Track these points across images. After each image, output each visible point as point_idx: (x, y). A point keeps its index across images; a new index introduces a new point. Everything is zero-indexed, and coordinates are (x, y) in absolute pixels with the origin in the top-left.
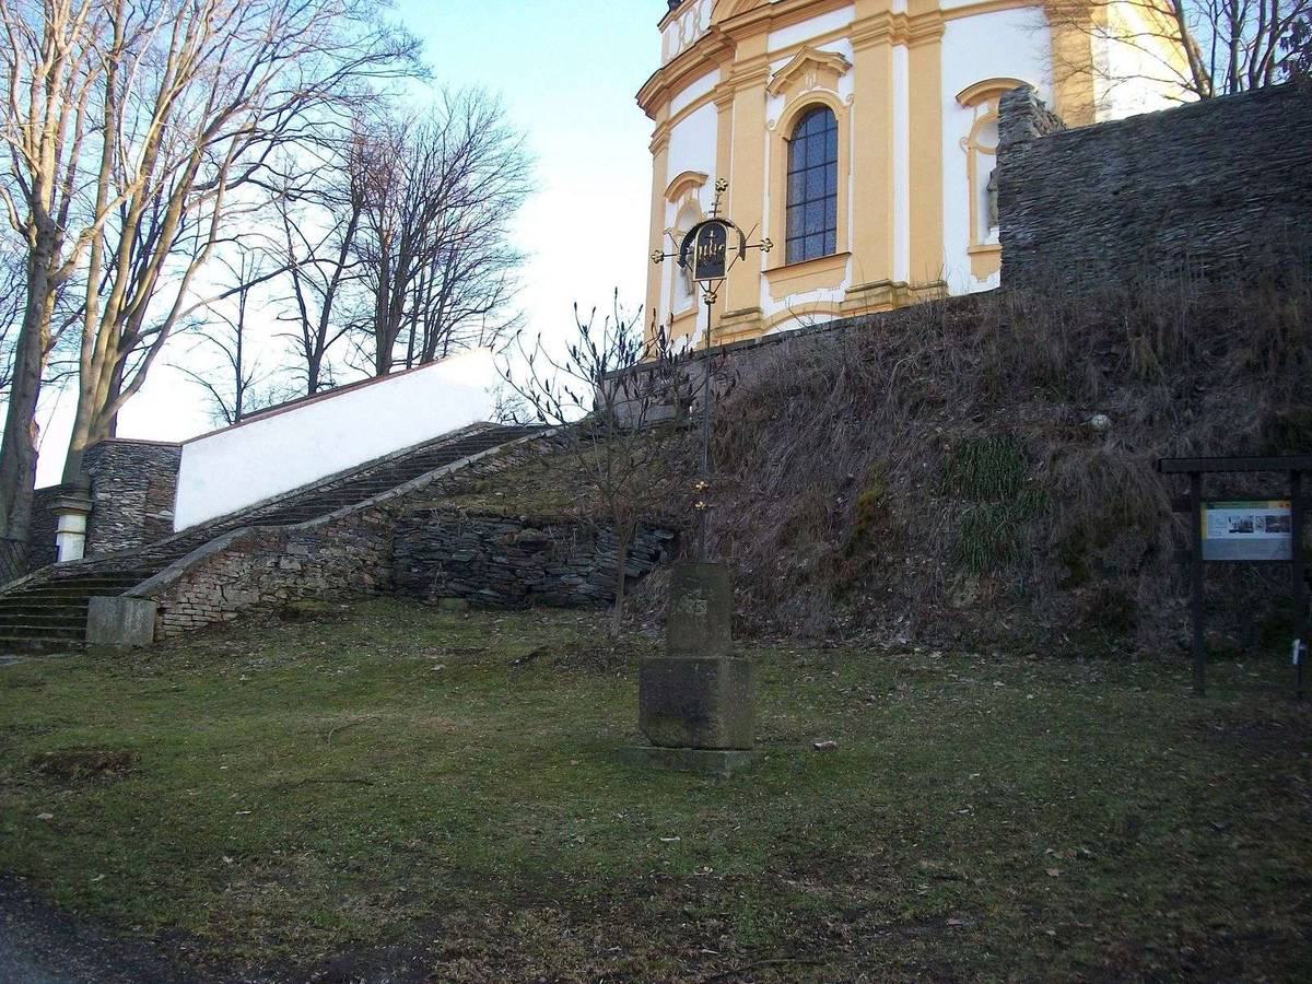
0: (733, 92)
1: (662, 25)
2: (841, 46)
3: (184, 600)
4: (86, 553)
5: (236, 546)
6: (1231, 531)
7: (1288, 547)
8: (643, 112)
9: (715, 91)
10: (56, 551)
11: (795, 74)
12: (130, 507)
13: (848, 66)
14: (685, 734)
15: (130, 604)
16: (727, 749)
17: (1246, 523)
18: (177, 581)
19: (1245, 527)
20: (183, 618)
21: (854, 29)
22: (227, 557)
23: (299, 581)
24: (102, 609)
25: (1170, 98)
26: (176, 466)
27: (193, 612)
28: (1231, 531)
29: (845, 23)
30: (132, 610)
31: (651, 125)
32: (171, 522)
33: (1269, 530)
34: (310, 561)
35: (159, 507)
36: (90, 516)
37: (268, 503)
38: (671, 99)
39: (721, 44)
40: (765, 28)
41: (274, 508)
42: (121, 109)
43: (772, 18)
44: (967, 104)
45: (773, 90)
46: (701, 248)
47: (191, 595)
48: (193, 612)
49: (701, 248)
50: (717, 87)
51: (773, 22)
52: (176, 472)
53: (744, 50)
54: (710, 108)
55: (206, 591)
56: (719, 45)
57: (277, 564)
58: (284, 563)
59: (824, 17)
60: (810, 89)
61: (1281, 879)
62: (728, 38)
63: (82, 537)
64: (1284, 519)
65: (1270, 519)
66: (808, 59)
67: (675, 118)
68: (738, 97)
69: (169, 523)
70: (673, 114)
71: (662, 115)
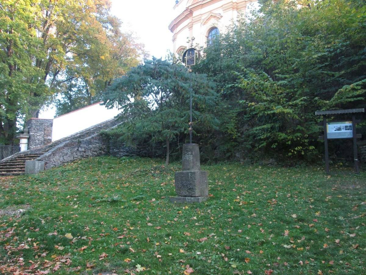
0: (192, 25)
1: (174, 8)
2: (220, 11)
3: (52, 160)
4: (28, 149)
5: (66, 146)
6: (335, 130)
7: (352, 134)
8: (170, 31)
9: (188, 25)
10: (20, 149)
11: (208, 19)
12: (39, 136)
13: (222, 17)
14: (187, 193)
15: (37, 162)
16: (200, 196)
17: (339, 128)
18: (50, 155)
20: (52, 165)
21: (223, 7)
22: (64, 148)
23: (84, 154)
24: (29, 163)
26: (51, 125)
27: (55, 163)
28: (335, 130)
29: (187, 24)
30: (37, 164)
31: (172, 34)
32: (51, 140)
33: (346, 129)
34: (87, 148)
35: (47, 136)
36: (29, 139)
37: (77, 134)
39: (189, 12)
40: (200, 7)
41: (79, 135)
43: (202, 5)
45: (203, 24)
47: (54, 159)
48: (55, 163)
50: (188, 24)
51: (202, 6)
52: (52, 127)
53: (195, 13)
54: (187, 29)
55: (59, 158)
56: (189, 12)
57: (78, 150)
58: (80, 149)
59: (184, 22)
60: (212, 22)
62: (191, 11)
63: (27, 145)
64: (350, 126)
65: (346, 127)
66: (211, 15)
67: (178, 32)
68: (194, 26)
69: (50, 140)
70: (177, 32)
71: (175, 31)
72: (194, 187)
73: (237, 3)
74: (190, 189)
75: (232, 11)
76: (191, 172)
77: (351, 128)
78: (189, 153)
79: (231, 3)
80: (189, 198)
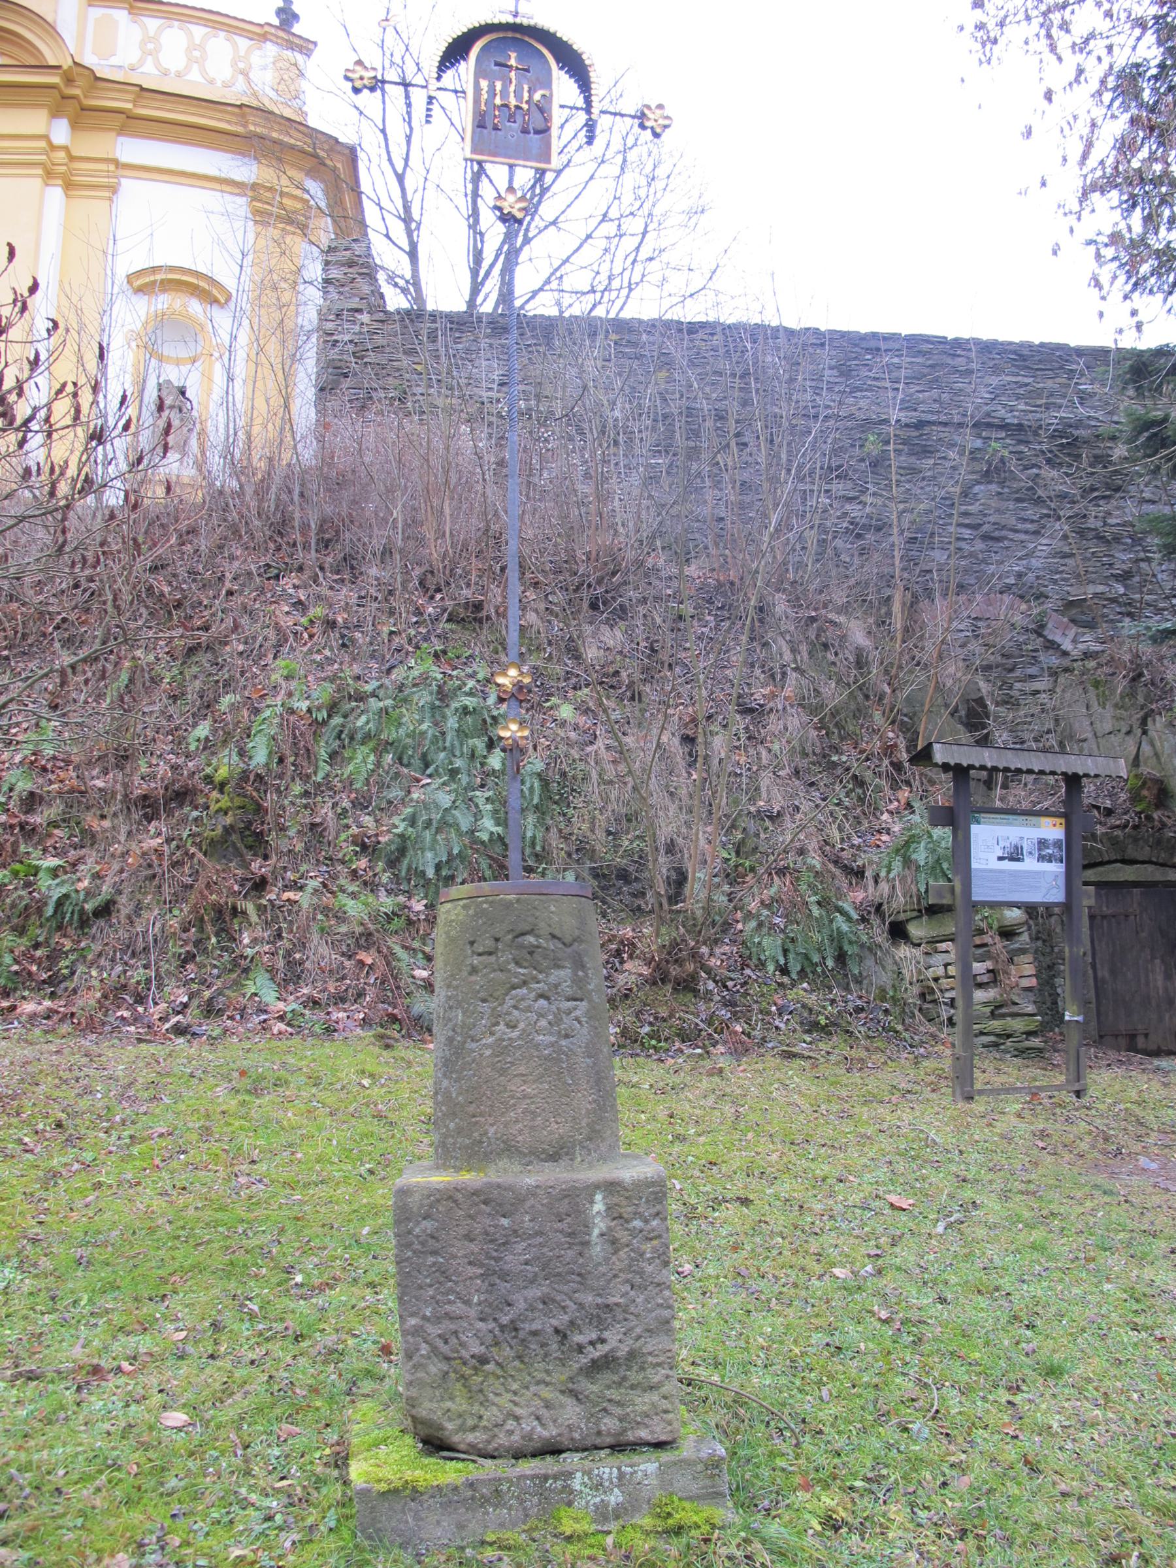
6: (1000, 859)
14: (571, 1413)
19: (1015, 855)
25: (101, 356)
28: (1000, 859)
33: (1041, 858)
37: (1011, 343)
38: (122, 131)
42: (149, 1041)
44: (139, 290)
46: (484, 84)
49: (484, 84)
61: (509, 1013)
64: (1057, 844)
65: (1042, 843)
72: (652, 1344)
73: (72, 158)
74: (596, 1367)
75: (39, 181)
76: (611, 1187)
77: (1058, 855)
78: (556, 975)
79: (43, 144)
80: (607, 1467)
